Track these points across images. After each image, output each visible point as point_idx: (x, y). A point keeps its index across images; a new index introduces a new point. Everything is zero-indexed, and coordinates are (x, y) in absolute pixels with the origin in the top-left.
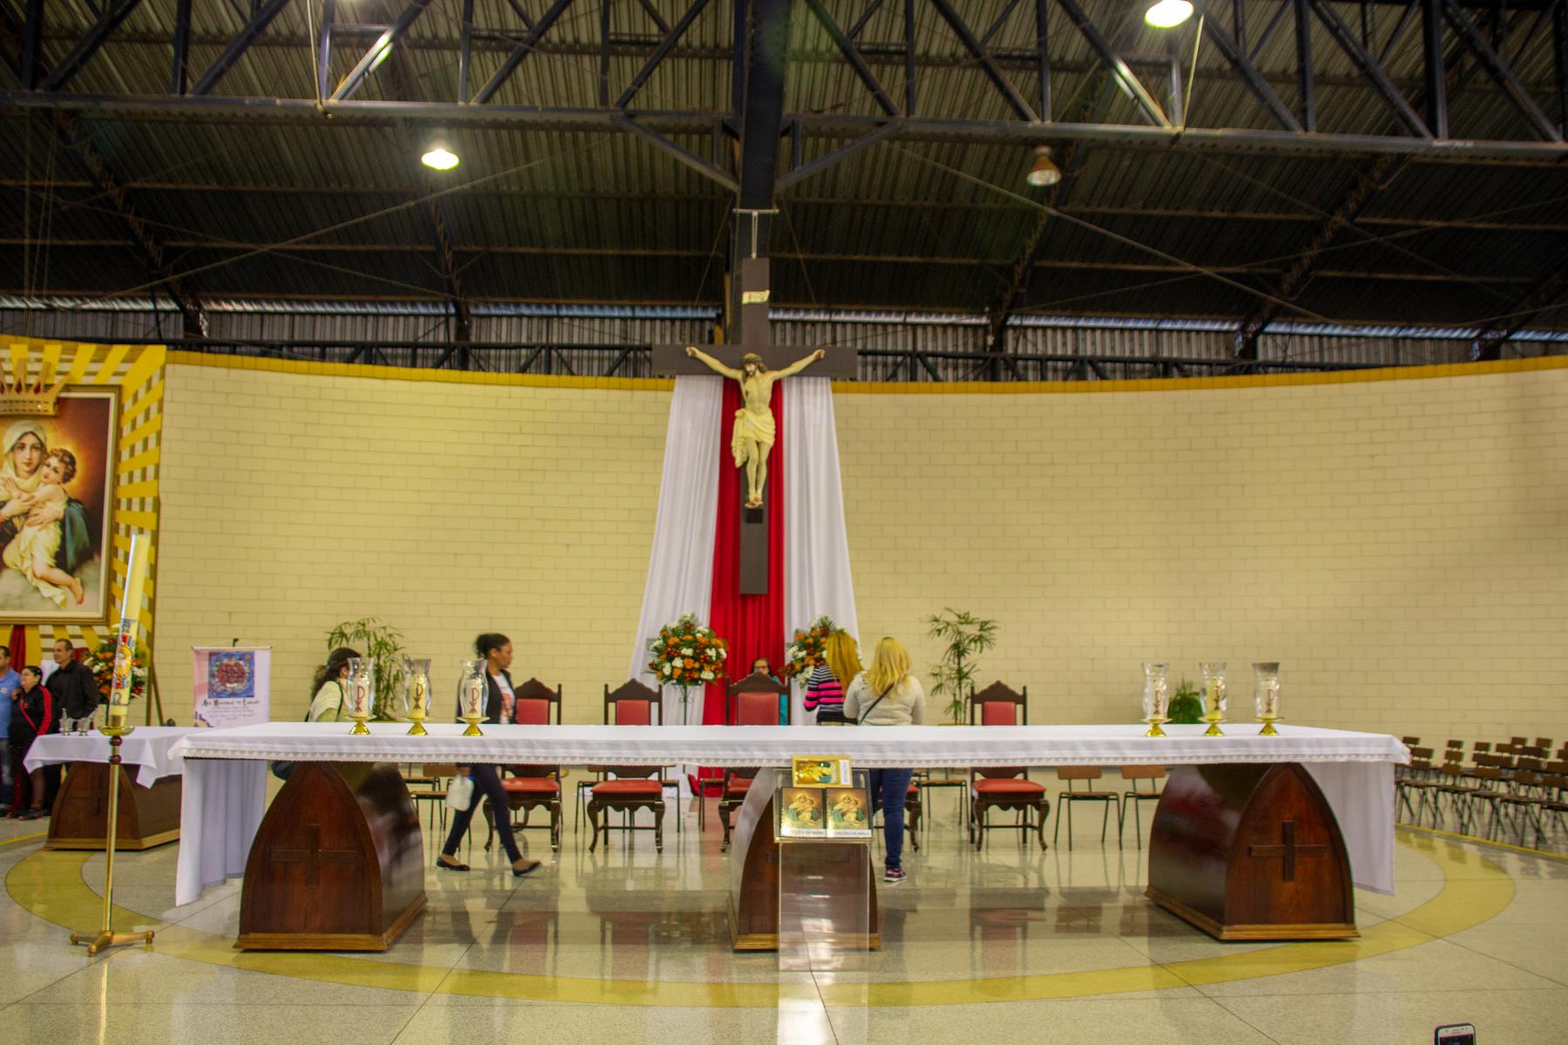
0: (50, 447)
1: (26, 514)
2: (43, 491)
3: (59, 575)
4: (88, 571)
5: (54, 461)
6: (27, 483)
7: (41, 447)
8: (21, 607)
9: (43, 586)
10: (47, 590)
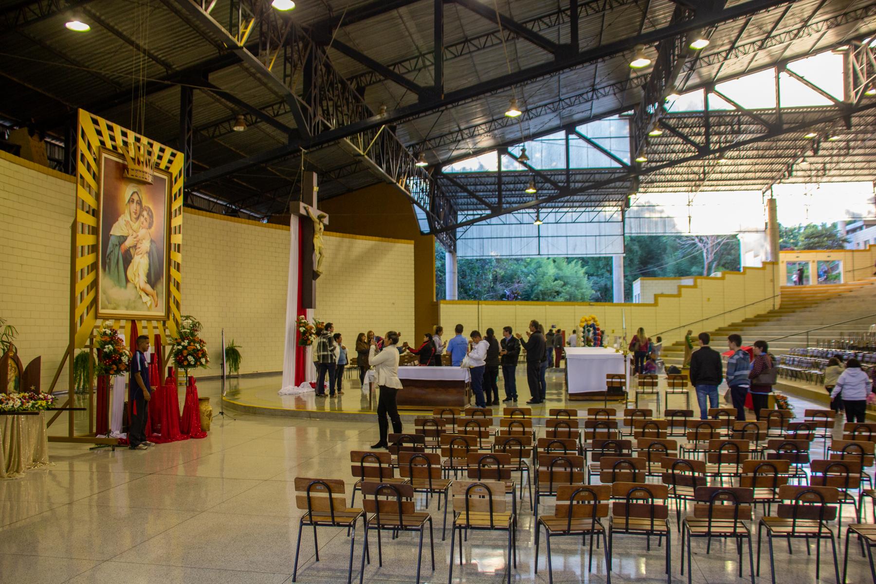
0: (144, 204)
1: (135, 247)
2: (142, 232)
3: (148, 288)
4: (159, 286)
5: (145, 213)
6: (135, 226)
7: (140, 203)
8: (134, 308)
9: (143, 294)
10: (146, 298)
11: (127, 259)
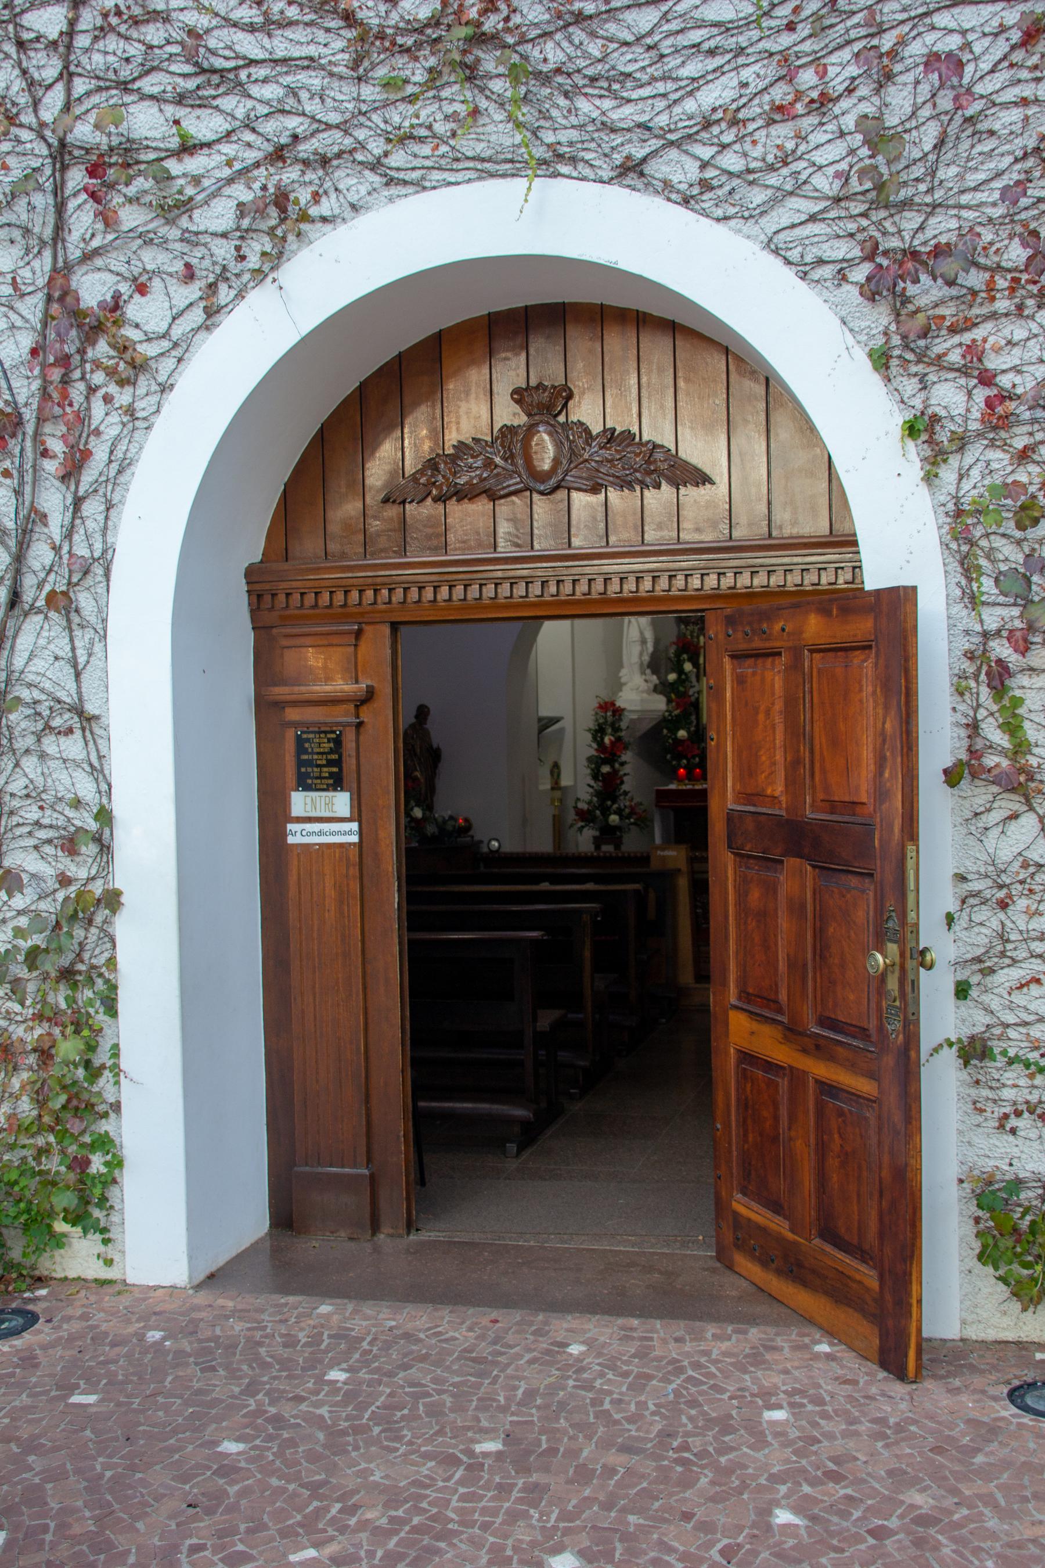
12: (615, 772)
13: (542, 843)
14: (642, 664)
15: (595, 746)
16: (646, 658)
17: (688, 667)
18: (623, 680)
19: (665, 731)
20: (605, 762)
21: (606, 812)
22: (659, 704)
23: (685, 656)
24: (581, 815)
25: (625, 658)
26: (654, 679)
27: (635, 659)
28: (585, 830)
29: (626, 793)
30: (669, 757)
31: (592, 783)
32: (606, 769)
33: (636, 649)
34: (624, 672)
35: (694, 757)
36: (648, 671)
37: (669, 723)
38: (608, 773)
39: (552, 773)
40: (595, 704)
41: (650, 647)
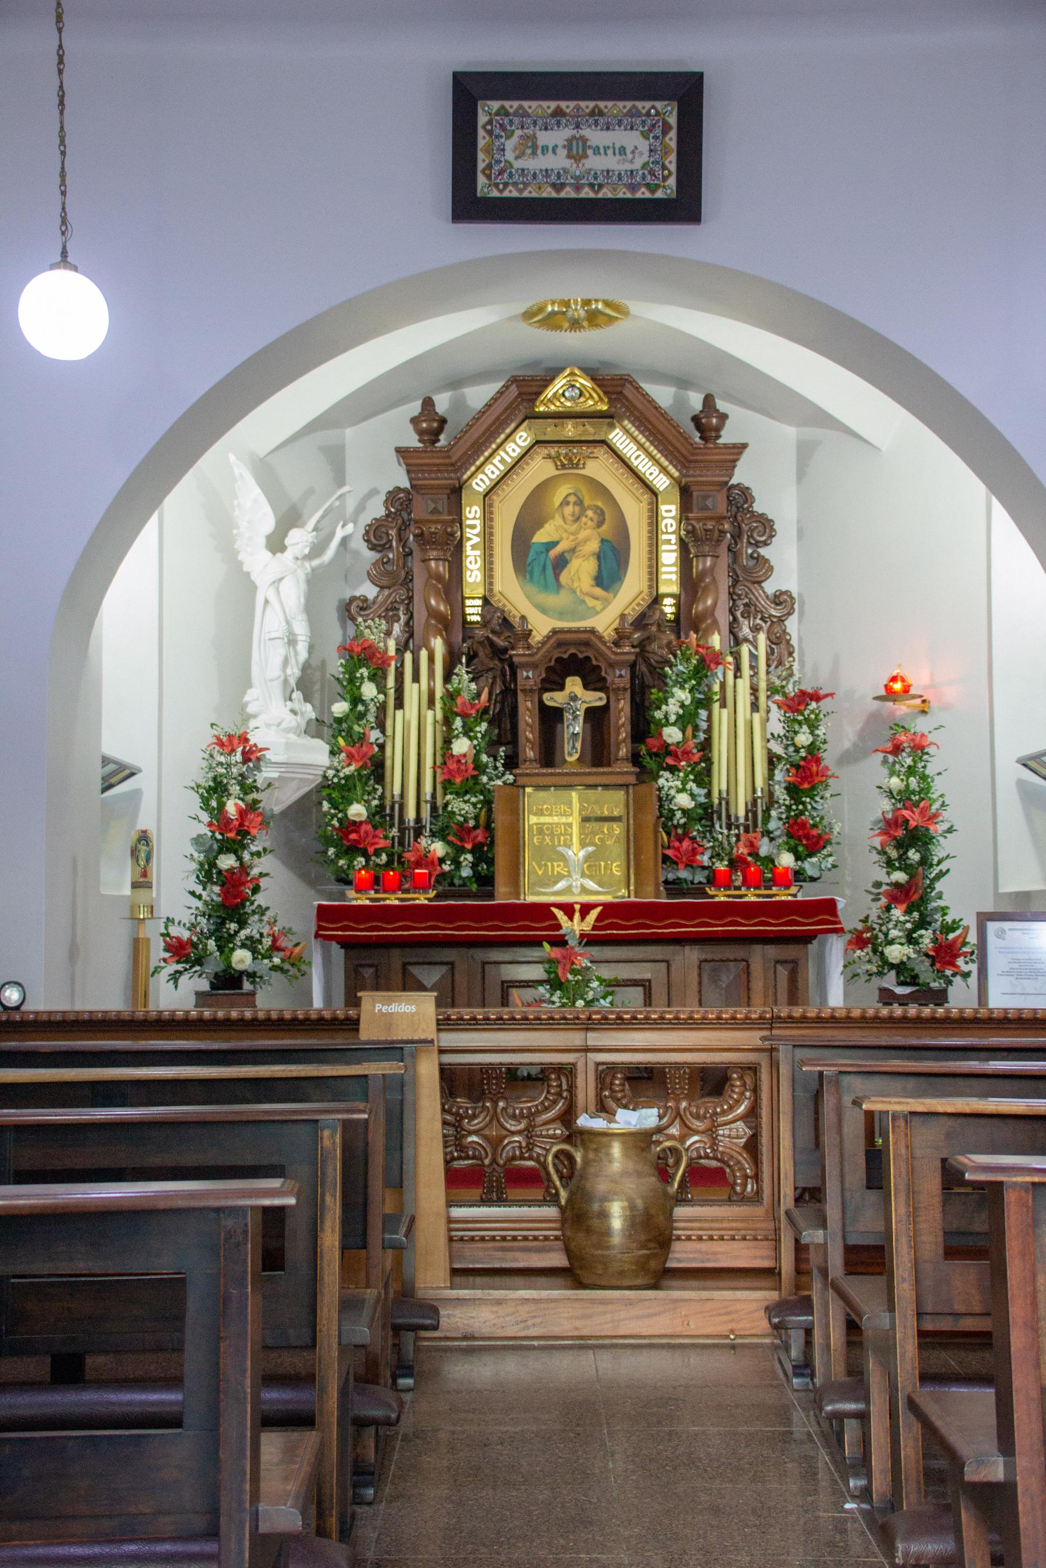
0: (587, 502)
1: (573, 550)
3: (598, 591)
5: (590, 513)
7: (580, 503)
11: (561, 563)
12: (244, 868)
13: (108, 998)
14: (286, 681)
15: (205, 817)
16: (294, 672)
17: (369, 690)
18: (250, 709)
19: (326, 806)
20: (226, 847)
21: (225, 944)
22: (318, 756)
23: (364, 672)
24: (178, 950)
25: (255, 668)
26: (309, 711)
27: (274, 670)
28: (184, 979)
29: (262, 911)
30: (331, 851)
31: (199, 889)
32: (227, 862)
33: (278, 652)
34: (250, 695)
35: (377, 853)
36: (297, 695)
37: (336, 791)
38: (231, 871)
39: (134, 853)
40: (207, 737)
41: (303, 655)
